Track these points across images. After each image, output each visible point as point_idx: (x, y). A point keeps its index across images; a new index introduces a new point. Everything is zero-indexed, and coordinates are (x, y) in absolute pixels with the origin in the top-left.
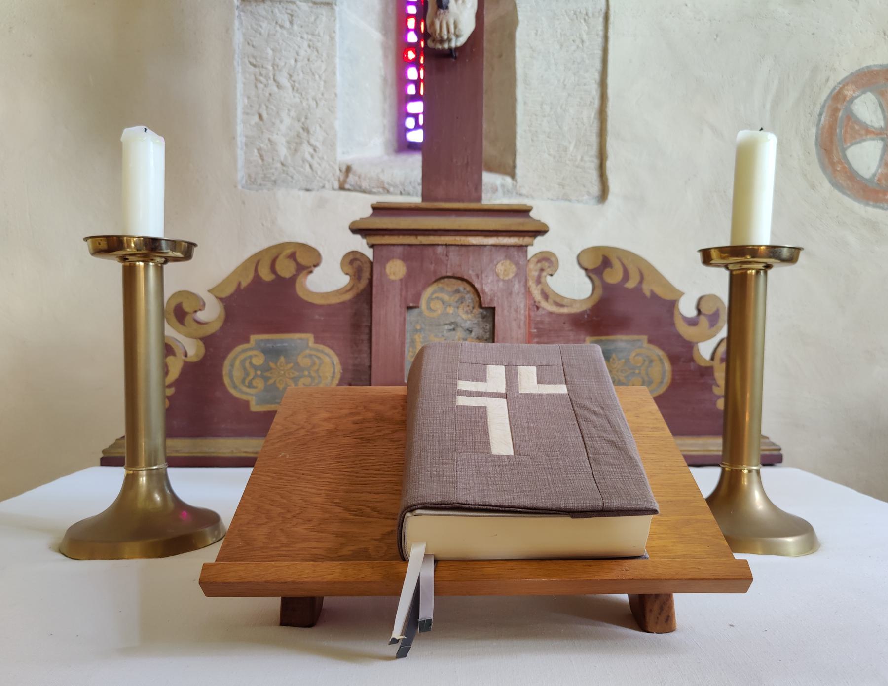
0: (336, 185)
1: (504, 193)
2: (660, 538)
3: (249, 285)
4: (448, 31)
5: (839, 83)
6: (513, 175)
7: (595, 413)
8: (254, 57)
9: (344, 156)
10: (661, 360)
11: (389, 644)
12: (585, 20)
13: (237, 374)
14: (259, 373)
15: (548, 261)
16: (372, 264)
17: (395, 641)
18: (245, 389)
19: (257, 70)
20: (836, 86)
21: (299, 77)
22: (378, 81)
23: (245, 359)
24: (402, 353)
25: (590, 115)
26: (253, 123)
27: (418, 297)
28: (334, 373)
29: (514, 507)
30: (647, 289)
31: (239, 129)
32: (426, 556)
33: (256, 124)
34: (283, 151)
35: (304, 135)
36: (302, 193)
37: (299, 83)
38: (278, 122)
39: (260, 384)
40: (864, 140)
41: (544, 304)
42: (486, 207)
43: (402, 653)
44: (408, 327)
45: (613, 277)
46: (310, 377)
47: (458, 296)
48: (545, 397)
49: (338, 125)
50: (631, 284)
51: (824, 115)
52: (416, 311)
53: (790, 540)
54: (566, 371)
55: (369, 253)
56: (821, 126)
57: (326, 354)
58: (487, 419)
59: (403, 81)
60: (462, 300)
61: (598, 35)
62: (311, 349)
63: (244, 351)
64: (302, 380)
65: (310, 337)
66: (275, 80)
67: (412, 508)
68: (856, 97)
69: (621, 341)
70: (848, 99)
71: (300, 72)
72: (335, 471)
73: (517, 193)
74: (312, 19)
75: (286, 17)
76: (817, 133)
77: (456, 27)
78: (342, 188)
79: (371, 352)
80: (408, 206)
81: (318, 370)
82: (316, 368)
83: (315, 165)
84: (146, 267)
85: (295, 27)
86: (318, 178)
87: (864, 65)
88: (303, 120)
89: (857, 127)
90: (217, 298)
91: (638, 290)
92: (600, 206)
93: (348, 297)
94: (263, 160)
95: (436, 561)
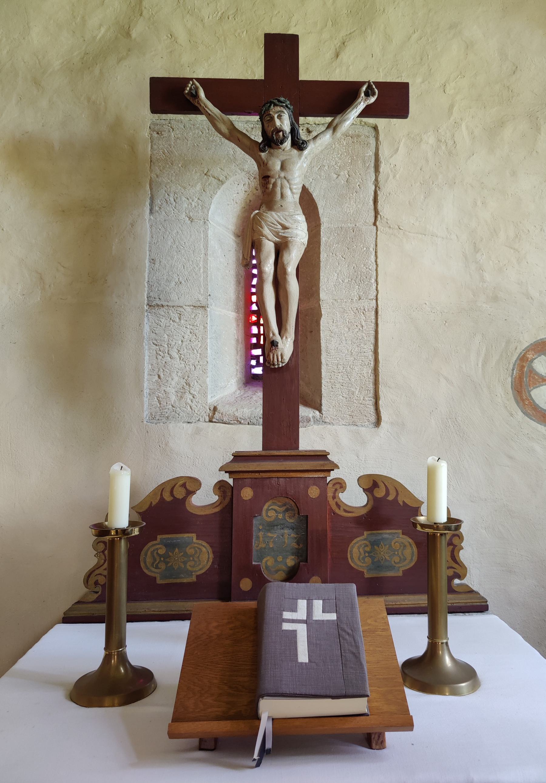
0: (207, 419)
1: (314, 422)
2: (377, 701)
3: (157, 503)
4: (278, 360)
5: (524, 350)
6: (320, 411)
7: (348, 634)
9: (211, 400)
10: (410, 545)
13: (149, 560)
15: (340, 485)
16: (232, 488)
17: (255, 760)
18: (153, 569)
19: (158, 347)
20: (521, 352)
21: (184, 351)
22: (233, 342)
23: (154, 551)
25: (368, 371)
26: (154, 381)
28: (209, 558)
29: (307, 695)
30: (400, 501)
31: (146, 385)
32: (269, 717)
34: (173, 398)
35: (187, 387)
36: (185, 425)
37: (184, 356)
39: (163, 566)
42: (301, 454)
43: (258, 765)
45: (380, 493)
46: (194, 561)
48: (325, 622)
50: (390, 498)
51: (516, 370)
53: (463, 684)
54: (337, 603)
55: (231, 481)
57: (204, 546)
58: (296, 638)
59: (248, 335)
61: (372, 322)
64: (189, 564)
65: (193, 536)
66: (168, 354)
67: (263, 696)
68: (535, 359)
69: (386, 533)
70: (529, 360)
71: (185, 348)
72: (222, 662)
73: (323, 421)
74: (193, 317)
75: (177, 316)
76: (512, 381)
77: (282, 358)
78: (211, 421)
81: (199, 556)
83: (194, 407)
85: (182, 321)
86: (195, 414)
87: (539, 338)
90: (137, 512)
91: (396, 500)
92: (376, 428)
93: (217, 510)
94: (160, 404)
95: (273, 719)
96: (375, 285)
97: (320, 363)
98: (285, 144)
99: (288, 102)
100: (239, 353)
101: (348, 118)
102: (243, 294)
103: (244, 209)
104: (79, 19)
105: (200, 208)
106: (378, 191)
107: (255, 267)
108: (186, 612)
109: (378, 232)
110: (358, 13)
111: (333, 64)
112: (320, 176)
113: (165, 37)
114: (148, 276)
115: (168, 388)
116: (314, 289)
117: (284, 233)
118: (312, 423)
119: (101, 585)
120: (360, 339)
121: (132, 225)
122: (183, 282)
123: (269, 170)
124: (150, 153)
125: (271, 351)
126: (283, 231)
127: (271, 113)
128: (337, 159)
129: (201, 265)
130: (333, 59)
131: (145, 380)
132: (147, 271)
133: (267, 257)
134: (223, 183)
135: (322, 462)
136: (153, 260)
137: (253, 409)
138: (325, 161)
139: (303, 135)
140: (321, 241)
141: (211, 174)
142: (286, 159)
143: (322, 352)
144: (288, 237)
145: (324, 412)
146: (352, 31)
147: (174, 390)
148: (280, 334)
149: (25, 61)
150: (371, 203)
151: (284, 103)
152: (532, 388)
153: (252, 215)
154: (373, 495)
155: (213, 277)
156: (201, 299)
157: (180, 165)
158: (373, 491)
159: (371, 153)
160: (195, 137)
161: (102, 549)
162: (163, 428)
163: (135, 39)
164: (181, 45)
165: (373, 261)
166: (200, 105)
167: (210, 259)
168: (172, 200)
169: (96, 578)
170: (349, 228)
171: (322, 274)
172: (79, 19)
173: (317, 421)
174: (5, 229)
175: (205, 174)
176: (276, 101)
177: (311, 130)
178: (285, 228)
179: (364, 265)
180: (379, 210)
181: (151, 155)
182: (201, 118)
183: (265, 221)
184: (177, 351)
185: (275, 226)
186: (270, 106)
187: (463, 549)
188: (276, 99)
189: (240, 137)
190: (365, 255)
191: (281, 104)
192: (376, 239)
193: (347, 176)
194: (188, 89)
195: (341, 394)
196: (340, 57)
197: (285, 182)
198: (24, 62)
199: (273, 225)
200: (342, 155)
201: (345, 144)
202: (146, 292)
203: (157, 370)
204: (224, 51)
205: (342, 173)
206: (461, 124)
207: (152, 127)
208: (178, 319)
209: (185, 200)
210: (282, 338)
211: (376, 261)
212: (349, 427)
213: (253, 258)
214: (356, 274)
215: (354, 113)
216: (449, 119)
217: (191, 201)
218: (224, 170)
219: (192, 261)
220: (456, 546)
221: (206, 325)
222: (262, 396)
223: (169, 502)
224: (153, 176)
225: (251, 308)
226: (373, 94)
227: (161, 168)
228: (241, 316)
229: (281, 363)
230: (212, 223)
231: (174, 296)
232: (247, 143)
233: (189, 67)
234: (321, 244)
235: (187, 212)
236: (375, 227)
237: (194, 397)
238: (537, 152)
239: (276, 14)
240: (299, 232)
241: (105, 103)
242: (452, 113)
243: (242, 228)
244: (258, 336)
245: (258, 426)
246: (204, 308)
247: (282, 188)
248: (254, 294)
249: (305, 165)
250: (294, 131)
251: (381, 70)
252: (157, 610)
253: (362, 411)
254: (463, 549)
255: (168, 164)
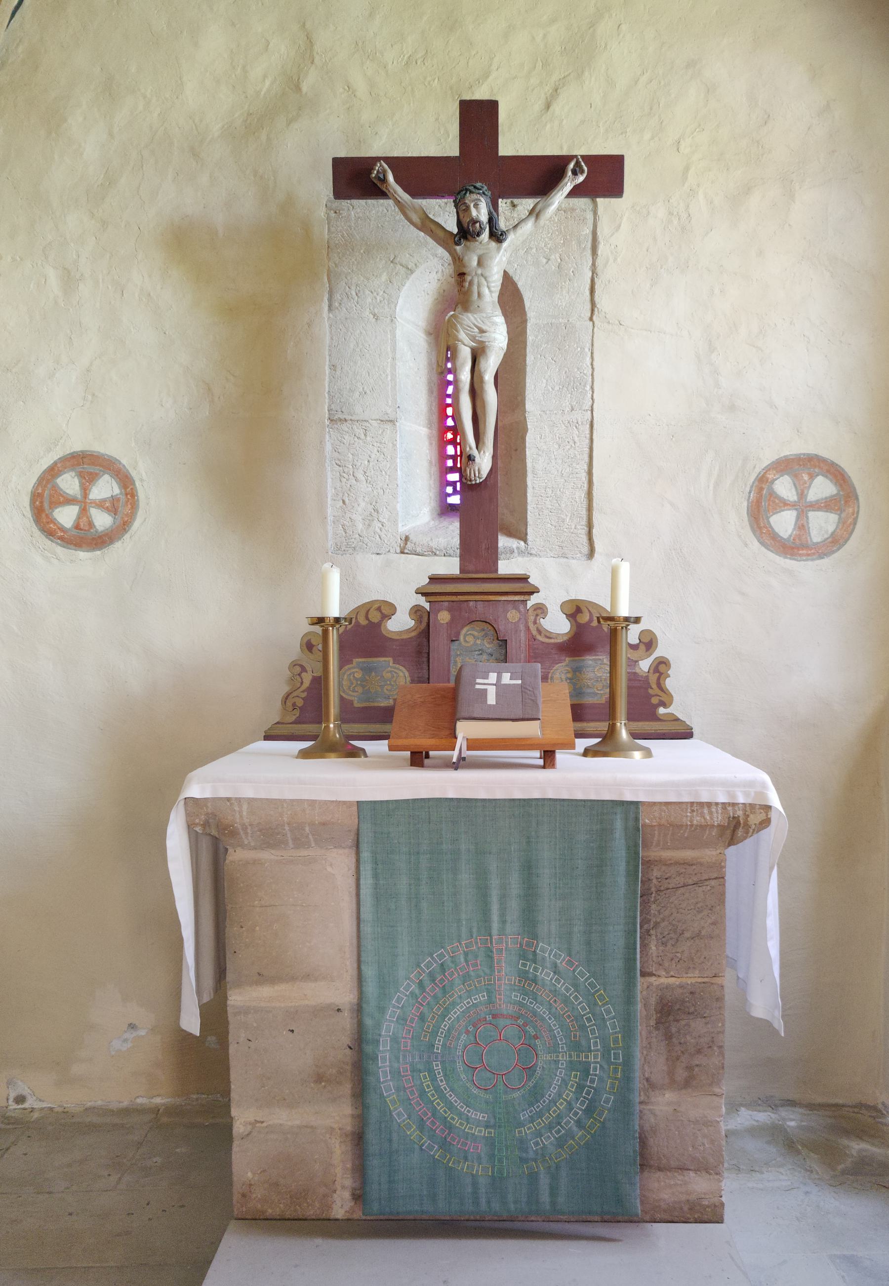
0: (398, 551)
4: (475, 476)
5: (763, 469)
6: (525, 541)
8: (339, 460)
9: (403, 528)
11: (505, 272)
12: (576, 427)
14: (359, 683)
16: (429, 613)
18: (351, 693)
24: (449, 670)
25: (581, 495)
27: (458, 634)
31: (329, 511)
32: (463, 737)
33: (341, 507)
34: (360, 526)
36: (374, 556)
38: (356, 505)
39: (360, 690)
40: (783, 511)
41: (539, 637)
42: (500, 577)
44: (452, 653)
45: (584, 618)
47: (483, 633)
49: (399, 507)
52: (457, 642)
55: (427, 606)
56: (750, 500)
57: (400, 670)
59: (443, 456)
60: (486, 635)
61: (586, 437)
62: (391, 667)
63: (349, 669)
65: (390, 660)
68: (776, 479)
70: (769, 480)
73: (528, 553)
74: (380, 432)
75: (362, 431)
76: (748, 505)
77: (479, 473)
78: (402, 552)
79: (429, 669)
80: (451, 576)
82: (394, 679)
83: (383, 536)
84: (333, 629)
85: (368, 438)
87: (782, 455)
88: (374, 503)
89: (777, 501)
92: (589, 561)
93: (413, 634)
94: (346, 533)
96: (591, 393)
97: (526, 486)
98: (483, 236)
99: (486, 188)
100: (433, 477)
101: (552, 202)
102: (437, 406)
103: (437, 301)
104: (239, 69)
105: (387, 303)
106: (596, 279)
107: (450, 371)
108: (384, 734)
109: (595, 329)
110: (574, 51)
111: (543, 117)
112: (526, 261)
113: (341, 90)
114: (329, 385)
115: (354, 515)
116: (519, 398)
117: (481, 337)
118: (516, 554)
119: (299, 707)
120: (572, 458)
121: (309, 325)
122: (368, 392)
123: (464, 266)
124: (326, 236)
125: (467, 465)
126: (480, 335)
127: (466, 201)
128: (547, 239)
129: (388, 372)
130: (543, 112)
131: (329, 506)
132: (327, 380)
133: (463, 364)
134: (412, 272)
135: (522, 585)
136: (333, 366)
137: (450, 538)
138: (533, 243)
139: (502, 224)
140: (528, 341)
141: (399, 262)
142: (484, 254)
143: (528, 473)
144: (485, 342)
145: (529, 543)
146: (566, 74)
147: (361, 517)
148: (477, 448)
149: (180, 126)
150: (587, 293)
151: (480, 189)
152: (771, 514)
153: (447, 318)
154: (576, 621)
155: (402, 386)
156: (389, 412)
157: (362, 251)
158: (576, 617)
159: (587, 231)
160: (379, 216)
161: (299, 672)
162: (349, 560)
163: (306, 93)
164: (360, 100)
165: (589, 364)
166: (389, 191)
167: (398, 364)
168: (354, 294)
169: (294, 700)
170: (560, 323)
171: (528, 381)
172: (239, 69)
173: (521, 553)
174: (167, 333)
175: (392, 262)
176: (471, 188)
177: (516, 203)
178: (482, 331)
179: (578, 369)
180: (596, 302)
181: (328, 239)
182: (391, 202)
183: (461, 324)
184: (363, 473)
185: (472, 330)
186: (465, 194)
187: (669, 677)
188: (472, 185)
189: (433, 227)
190: (579, 357)
191: (477, 191)
192: (593, 337)
193: (559, 260)
194: (375, 172)
195: (549, 522)
196: (551, 109)
197: (483, 280)
198: (179, 128)
199: (469, 329)
200: (553, 235)
201: (556, 220)
202: (327, 404)
203: (341, 495)
204: (412, 104)
205: (553, 257)
206: (698, 192)
207: (329, 204)
208: (363, 435)
209: (369, 294)
210: (479, 453)
211: (592, 365)
212: (558, 560)
213: (448, 360)
214: (568, 380)
215: (559, 197)
216: (683, 185)
217: (375, 294)
218: (413, 257)
219: (379, 367)
220: (662, 673)
221: (395, 442)
222: (459, 527)
223: (364, 627)
224: (331, 264)
225: (446, 423)
226: (582, 172)
227: (340, 255)
228: (435, 432)
229: (478, 479)
230: (399, 320)
231: (358, 409)
232: (441, 234)
233: (370, 127)
234: (528, 344)
235: (371, 308)
236: (591, 323)
237: (383, 525)
238: (789, 225)
239: (473, 54)
240: (497, 336)
241: (274, 177)
242: (687, 178)
243: (434, 324)
244: (454, 458)
245: (455, 558)
246: (392, 422)
247: (479, 286)
248: (449, 405)
249: (504, 259)
250: (491, 221)
251: (601, 125)
252: (355, 731)
253: (573, 542)
254: (669, 677)
255: (348, 250)
